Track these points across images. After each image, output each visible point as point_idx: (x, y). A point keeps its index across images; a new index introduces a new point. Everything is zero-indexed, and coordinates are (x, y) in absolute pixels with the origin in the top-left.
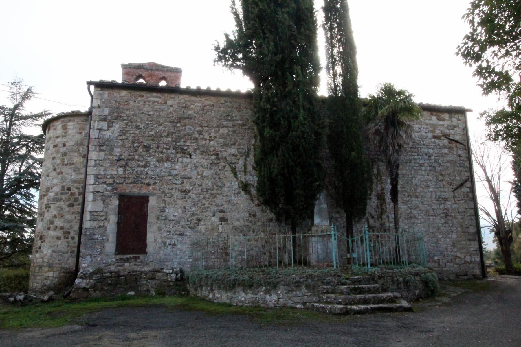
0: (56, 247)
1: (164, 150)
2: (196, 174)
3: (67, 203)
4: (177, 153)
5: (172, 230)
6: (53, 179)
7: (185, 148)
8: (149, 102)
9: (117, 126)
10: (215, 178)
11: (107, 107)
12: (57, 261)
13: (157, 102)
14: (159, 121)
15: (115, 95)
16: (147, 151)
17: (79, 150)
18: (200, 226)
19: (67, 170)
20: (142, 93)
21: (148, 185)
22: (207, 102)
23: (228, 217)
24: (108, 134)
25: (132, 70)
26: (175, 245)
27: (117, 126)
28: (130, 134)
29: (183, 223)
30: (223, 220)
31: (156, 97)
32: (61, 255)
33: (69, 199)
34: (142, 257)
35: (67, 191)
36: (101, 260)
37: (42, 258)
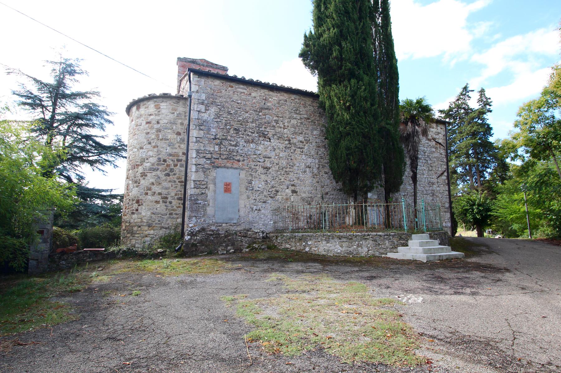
0: (155, 210)
2: (274, 155)
3: (164, 173)
4: (260, 136)
5: (258, 198)
7: (266, 133)
9: (213, 110)
10: (288, 159)
11: (204, 93)
12: (157, 222)
15: (210, 83)
16: (237, 133)
18: (278, 196)
19: (161, 144)
20: (232, 84)
21: (239, 161)
22: (281, 98)
23: (298, 190)
24: (205, 116)
25: (187, 64)
26: (260, 210)
27: (213, 110)
29: (265, 193)
30: (294, 192)
31: (241, 88)
33: (166, 170)
36: (205, 221)
37: (141, 219)
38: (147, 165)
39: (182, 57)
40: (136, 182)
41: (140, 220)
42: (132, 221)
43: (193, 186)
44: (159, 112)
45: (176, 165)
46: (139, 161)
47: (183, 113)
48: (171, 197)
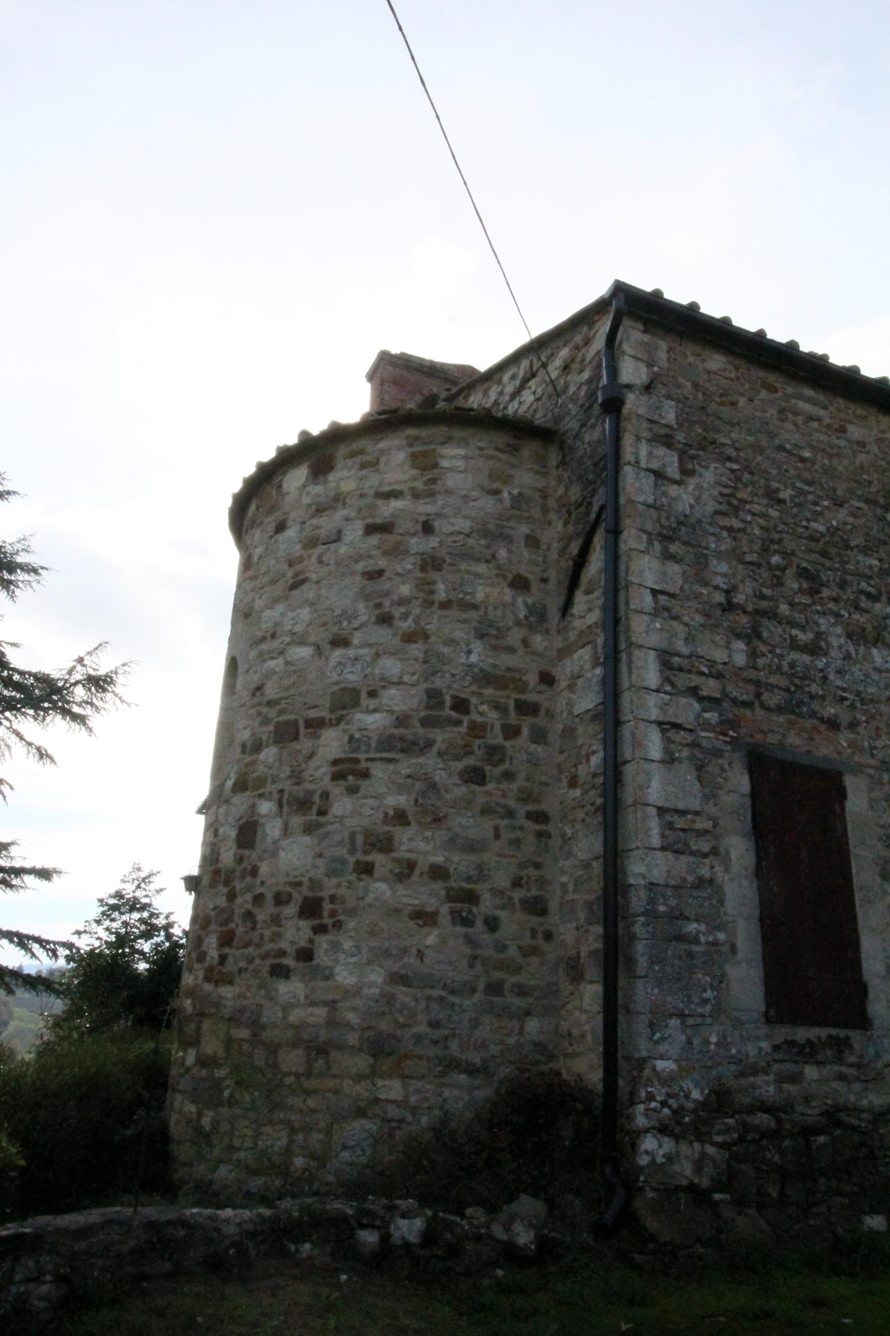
0: (411, 960)
1: (863, 598)
6: (377, 655)
8: (796, 414)
11: (669, 397)
12: (422, 1028)
13: (819, 420)
14: (835, 491)
15: (691, 359)
17: (494, 556)
21: (833, 724)
24: (683, 498)
28: (753, 514)
31: (809, 400)
32: (441, 1000)
34: (856, 1037)
35: (453, 714)
37: (332, 1004)
38: (371, 721)
39: (395, 350)
40: (303, 804)
41: (321, 1012)
42: (271, 1015)
43: (656, 841)
44: (433, 481)
45: (511, 732)
46: (327, 702)
47: (537, 497)
48: (498, 893)
